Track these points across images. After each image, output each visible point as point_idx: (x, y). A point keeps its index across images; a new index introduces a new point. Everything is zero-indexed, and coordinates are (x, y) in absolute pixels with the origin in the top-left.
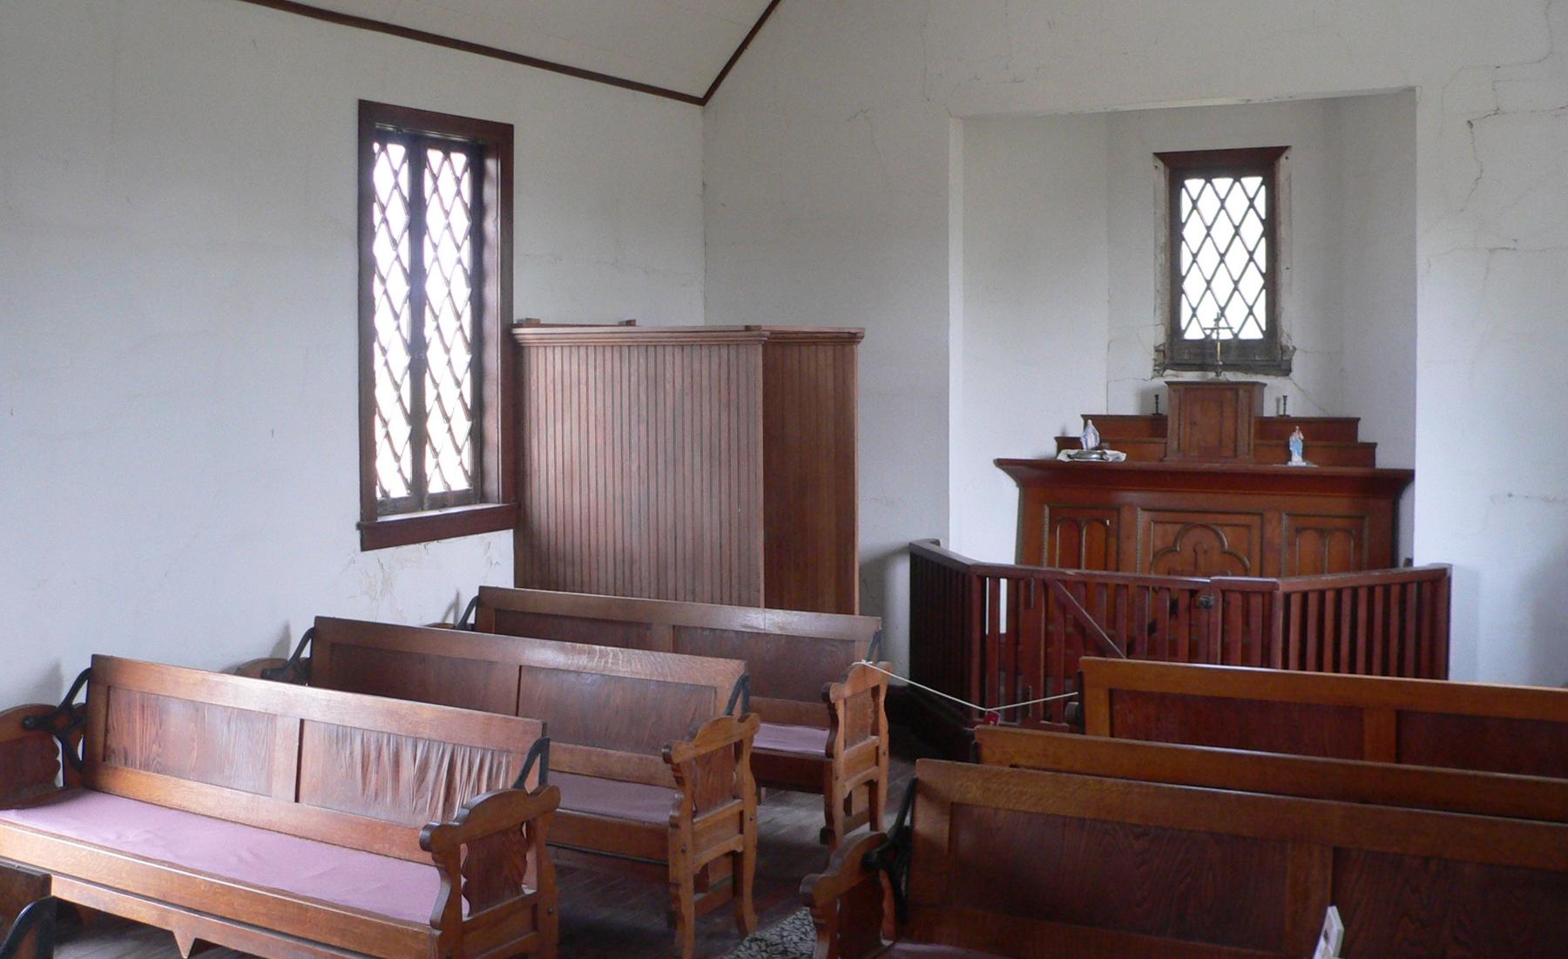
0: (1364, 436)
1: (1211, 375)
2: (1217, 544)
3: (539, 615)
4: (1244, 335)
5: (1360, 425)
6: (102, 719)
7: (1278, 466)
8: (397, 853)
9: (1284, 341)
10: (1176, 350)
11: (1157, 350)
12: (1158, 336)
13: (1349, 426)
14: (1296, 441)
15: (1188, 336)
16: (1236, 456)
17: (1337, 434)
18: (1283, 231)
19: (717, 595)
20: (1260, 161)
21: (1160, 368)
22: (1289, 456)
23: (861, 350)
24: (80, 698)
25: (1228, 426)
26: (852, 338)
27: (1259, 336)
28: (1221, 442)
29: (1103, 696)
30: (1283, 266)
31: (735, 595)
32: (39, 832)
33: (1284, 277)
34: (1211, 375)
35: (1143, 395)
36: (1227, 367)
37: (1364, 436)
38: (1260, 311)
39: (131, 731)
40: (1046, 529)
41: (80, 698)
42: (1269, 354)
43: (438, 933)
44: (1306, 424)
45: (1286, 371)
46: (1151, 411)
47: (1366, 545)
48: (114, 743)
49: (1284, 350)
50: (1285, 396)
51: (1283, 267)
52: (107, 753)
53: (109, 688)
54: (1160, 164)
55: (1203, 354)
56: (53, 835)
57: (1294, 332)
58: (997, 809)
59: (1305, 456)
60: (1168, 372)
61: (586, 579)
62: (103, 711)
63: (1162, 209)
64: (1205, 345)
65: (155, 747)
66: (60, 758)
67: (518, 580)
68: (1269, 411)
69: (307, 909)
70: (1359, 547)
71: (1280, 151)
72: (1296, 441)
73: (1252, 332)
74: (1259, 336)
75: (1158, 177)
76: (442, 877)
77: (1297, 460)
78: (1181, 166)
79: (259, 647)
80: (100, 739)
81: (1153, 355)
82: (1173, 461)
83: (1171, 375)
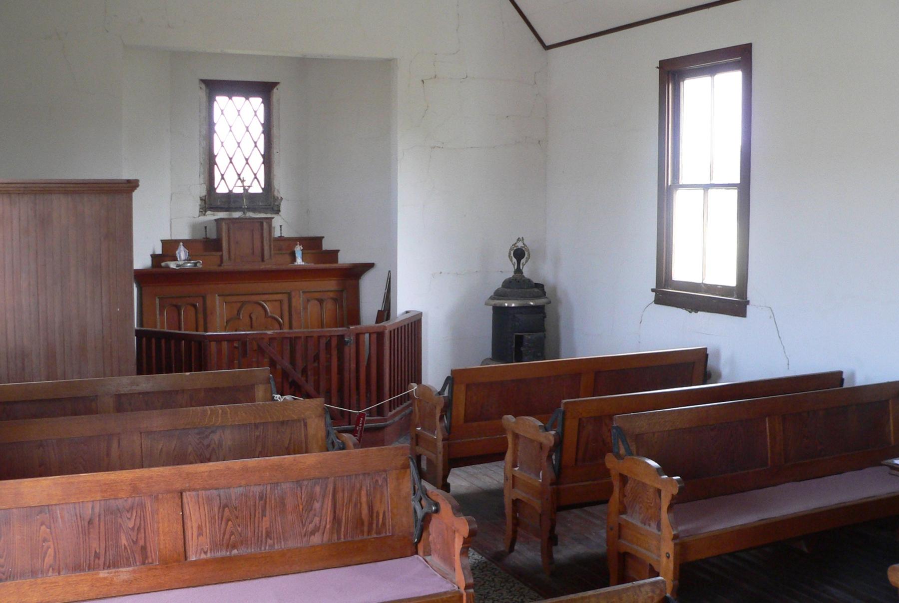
0: (327, 246)
1: (236, 215)
2: (262, 312)
4: (251, 191)
5: (323, 240)
7: (290, 266)
8: (298, 568)
9: (276, 194)
10: (212, 201)
11: (201, 199)
12: (202, 191)
13: (318, 240)
14: (298, 250)
15: (219, 191)
16: (263, 260)
17: (313, 244)
18: (275, 131)
20: (264, 90)
21: (204, 210)
22: (294, 259)
23: (135, 194)
25: (257, 243)
26: (132, 185)
27: (260, 191)
28: (253, 253)
29: (463, 388)
30: (275, 151)
33: (276, 157)
34: (236, 215)
35: (194, 227)
36: (249, 209)
37: (327, 246)
38: (261, 176)
40: (158, 312)
42: (268, 200)
43: (472, 591)
44: (186, 243)
45: (278, 212)
46: (200, 236)
47: (344, 305)
49: (275, 199)
50: (283, 225)
51: (275, 151)
54: (203, 86)
55: (230, 201)
57: (281, 188)
58: (654, 433)
59: (303, 260)
60: (209, 212)
63: (204, 113)
64: (230, 195)
68: (277, 234)
70: (341, 307)
71: (274, 84)
72: (298, 250)
73: (257, 189)
74: (260, 191)
75: (202, 94)
77: (299, 261)
78: (216, 87)
81: (199, 202)
82: (227, 266)
83: (211, 216)
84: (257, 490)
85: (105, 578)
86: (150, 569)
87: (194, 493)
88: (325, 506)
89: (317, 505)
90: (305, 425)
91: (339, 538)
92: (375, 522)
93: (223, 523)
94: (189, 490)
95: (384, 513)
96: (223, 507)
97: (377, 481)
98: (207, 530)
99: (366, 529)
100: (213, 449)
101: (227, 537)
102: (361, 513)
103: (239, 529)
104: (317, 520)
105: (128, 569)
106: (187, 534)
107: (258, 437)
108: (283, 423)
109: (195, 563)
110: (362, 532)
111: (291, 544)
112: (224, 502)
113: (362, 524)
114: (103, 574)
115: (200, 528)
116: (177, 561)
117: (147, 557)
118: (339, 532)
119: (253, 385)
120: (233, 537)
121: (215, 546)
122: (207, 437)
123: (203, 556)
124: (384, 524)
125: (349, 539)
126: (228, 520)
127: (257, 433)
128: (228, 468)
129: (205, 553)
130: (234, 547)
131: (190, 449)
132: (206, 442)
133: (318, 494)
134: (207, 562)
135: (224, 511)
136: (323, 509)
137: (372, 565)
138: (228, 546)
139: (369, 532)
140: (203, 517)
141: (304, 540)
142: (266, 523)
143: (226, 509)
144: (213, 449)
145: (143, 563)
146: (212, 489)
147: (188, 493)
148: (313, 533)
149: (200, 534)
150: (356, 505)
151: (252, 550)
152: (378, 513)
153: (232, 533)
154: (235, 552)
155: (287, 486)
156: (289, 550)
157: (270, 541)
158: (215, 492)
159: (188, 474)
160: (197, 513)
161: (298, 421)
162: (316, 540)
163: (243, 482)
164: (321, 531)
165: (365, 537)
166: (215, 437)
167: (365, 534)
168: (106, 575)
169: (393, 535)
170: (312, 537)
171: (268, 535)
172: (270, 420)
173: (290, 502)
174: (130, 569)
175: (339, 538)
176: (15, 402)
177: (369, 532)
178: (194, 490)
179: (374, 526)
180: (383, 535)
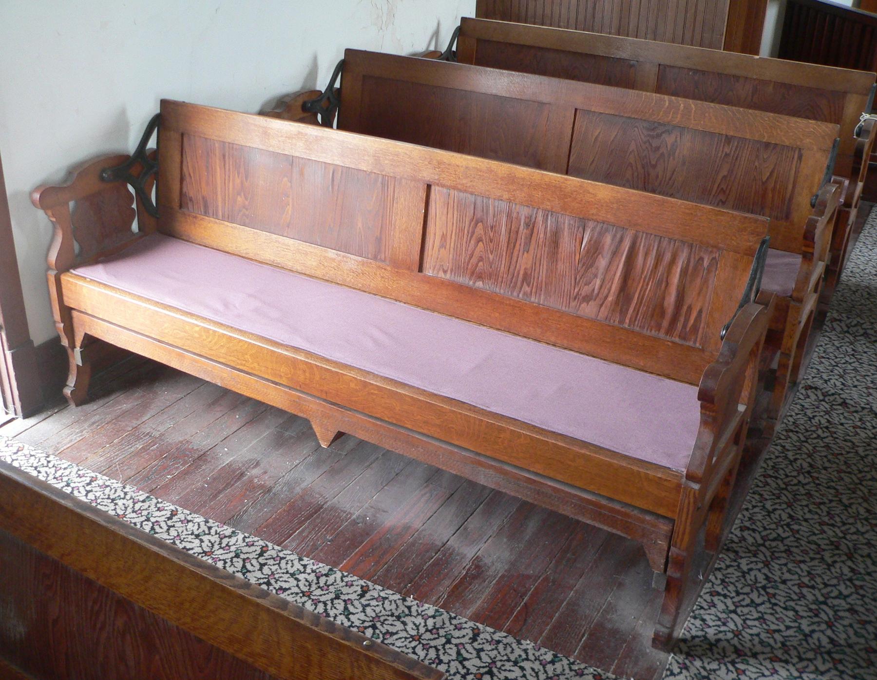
3: (523, 46)
6: (177, 165)
19: (688, 36)
24: (152, 144)
31: (697, 37)
32: (140, 298)
39: (209, 180)
41: (152, 144)
48: (191, 190)
52: (184, 201)
53: (182, 135)
56: (157, 303)
61: (548, 11)
62: (177, 158)
65: (240, 199)
66: (134, 206)
67: (478, 14)
69: (501, 429)
76: (704, 422)
79: (287, 80)
80: (176, 187)
84: (524, 212)
85: (333, 260)
86: (379, 267)
87: (445, 190)
88: (613, 268)
89: (602, 262)
90: (800, 157)
91: (622, 322)
92: (682, 319)
93: (472, 242)
94: (438, 185)
95: (700, 311)
96: (476, 221)
97: (701, 259)
98: (451, 243)
99: (665, 324)
100: (662, 154)
101: (474, 260)
102: (664, 298)
103: (491, 257)
104: (598, 282)
105: (357, 258)
106: (427, 239)
107: (727, 155)
108: (767, 145)
109: (429, 280)
110: (659, 327)
111: (554, 303)
112: (479, 214)
113: (663, 313)
114: (331, 253)
115: (444, 237)
116: (409, 269)
117: (379, 252)
118: (623, 313)
119: (845, 93)
120: (481, 264)
121: (458, 268)
122: (659, 136)
123: (441, 275)
124: (695, 329)
125: (637, 329)
126: (479, 240)
127: (727, 150)
128: (490, 171)
129: (445, 272)
130: (480, 277)
131: (633, 147)
132: (655, 143)
133: (606, 247)
134: (443, 284)
135: (476, 225)
136: (608, 272)
137: (687, 385)
138: (472, 273)
139: (670, 331)
140: (450, 224)
141: (573, 304)
142: (524, 262)
143: (480, 224)
144: (662, 154)
145: (375, 258)
146: (465, 191)
147: (437, 188)
148: (587, 299)
149: (443, 246)
150: (660, 282)
151: (501, 290)
152: (690, 308)
153: (481, 259)
154: (479, 284)
155: (567, 222)
156: (548, 310)
157: (526, 288)
158: (472, 198)
159: (440, 163)
160: (444, 218)
161: (791, 148)
162: (588, 310)
163: (506, 196)
164: (598, 302)
165: (662, 335)
166: (670, 139)
167: (663, 331)
168: (334, 256)
169: (703, 350)
170: (584, 305)
171: (527, 278)
172: (748, 137)
173: (566, 243)
174: (360, 259)
175: (622, 322)
176: (548, 50)
177: (670, 331)
178: (443, 186)
179: (680, 325)
180: (691, 344)
